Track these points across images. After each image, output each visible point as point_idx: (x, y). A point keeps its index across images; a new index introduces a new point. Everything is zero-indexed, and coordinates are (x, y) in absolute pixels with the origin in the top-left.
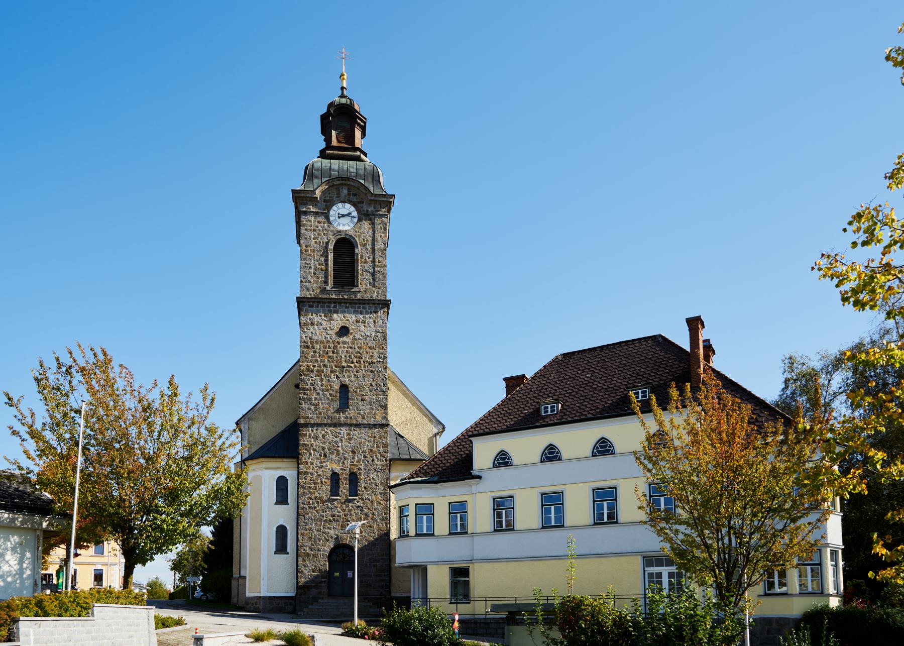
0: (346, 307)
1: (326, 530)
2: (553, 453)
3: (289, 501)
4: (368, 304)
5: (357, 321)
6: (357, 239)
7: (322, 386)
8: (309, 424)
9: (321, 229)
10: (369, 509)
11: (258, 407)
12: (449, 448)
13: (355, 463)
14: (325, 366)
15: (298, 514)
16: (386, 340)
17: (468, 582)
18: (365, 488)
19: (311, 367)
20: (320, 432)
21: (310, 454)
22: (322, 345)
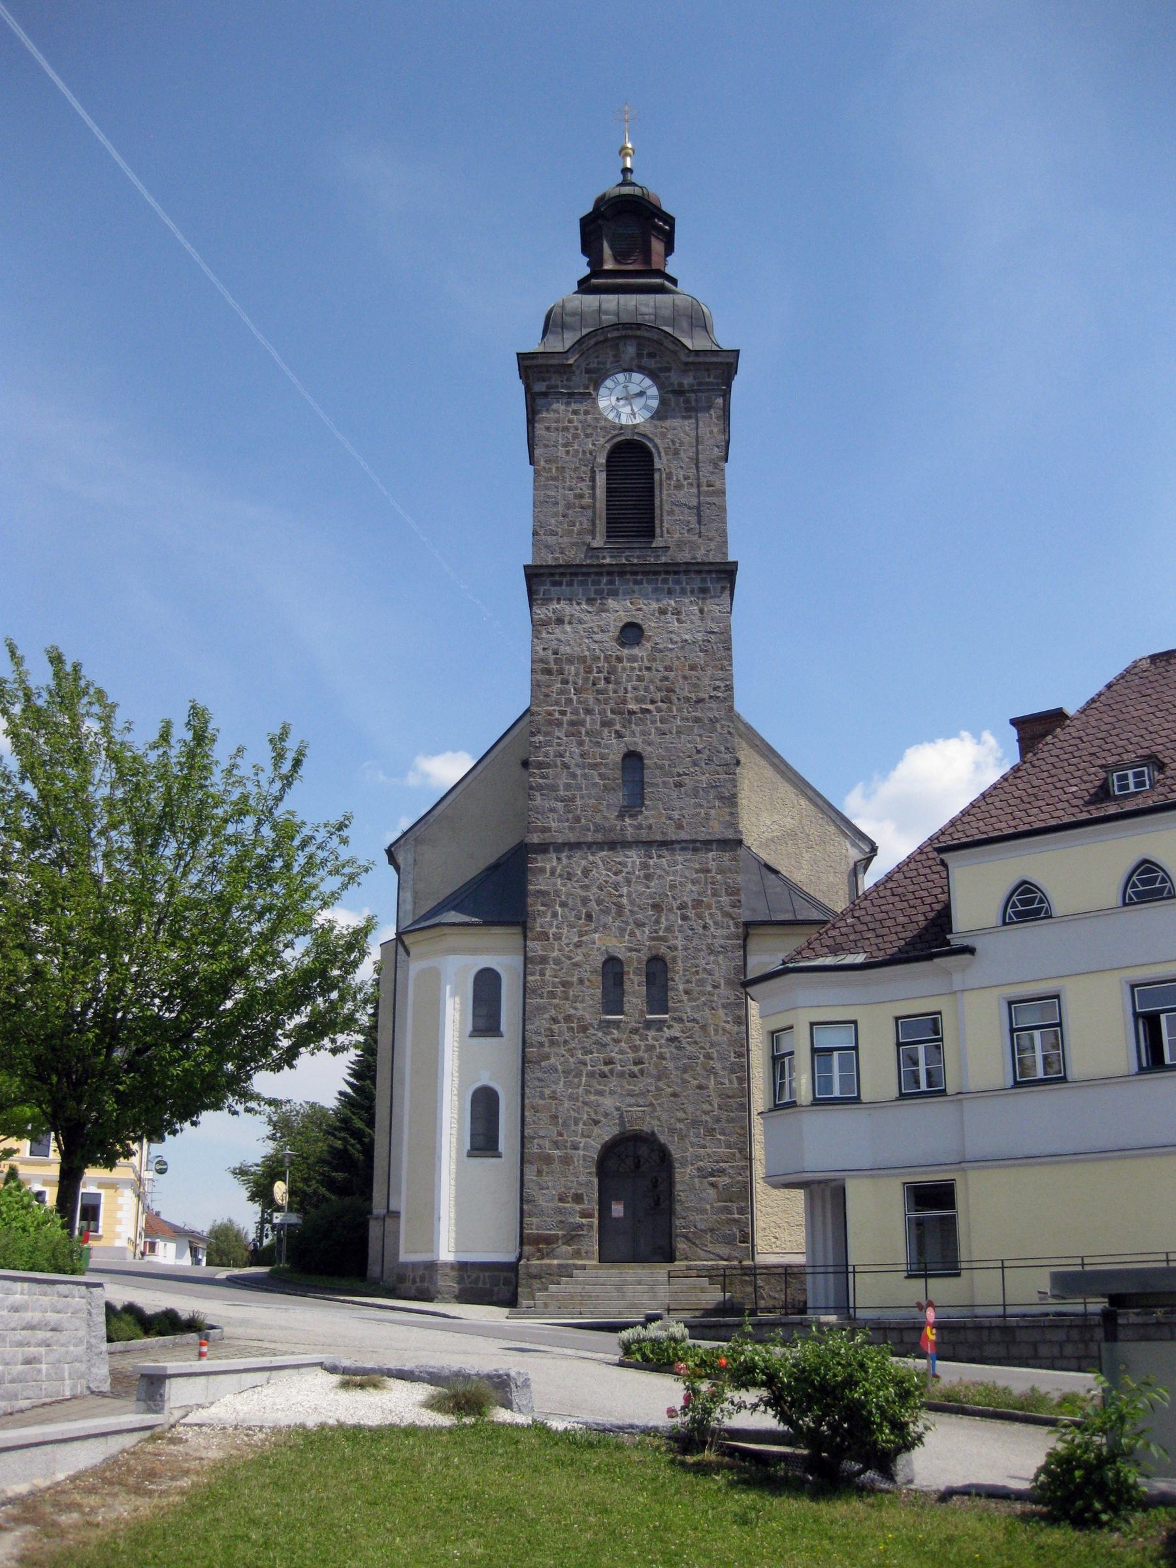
0: (636, 582)
1: (592, 1098)
2: (1153, 881)
3: (504, 1027)
4: (686, 572)
5: (663, 612)
6: (658, 441)
7: (582, 756)
8: (551, 843)
9: (580, 426)
10: (696, 1043)
11: (436, 812)
12: (890, 885)
13: (661, 933)
14: (588, 711)
15: (524, 1060)
16: (729, 649)
17: (952, 1219)
18: (686, 992)
19: (557, 715)
20: (579, 862)
21: (555, 915)
22: (582, 667)
